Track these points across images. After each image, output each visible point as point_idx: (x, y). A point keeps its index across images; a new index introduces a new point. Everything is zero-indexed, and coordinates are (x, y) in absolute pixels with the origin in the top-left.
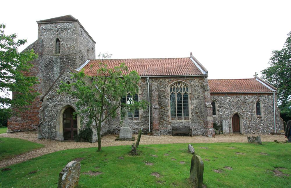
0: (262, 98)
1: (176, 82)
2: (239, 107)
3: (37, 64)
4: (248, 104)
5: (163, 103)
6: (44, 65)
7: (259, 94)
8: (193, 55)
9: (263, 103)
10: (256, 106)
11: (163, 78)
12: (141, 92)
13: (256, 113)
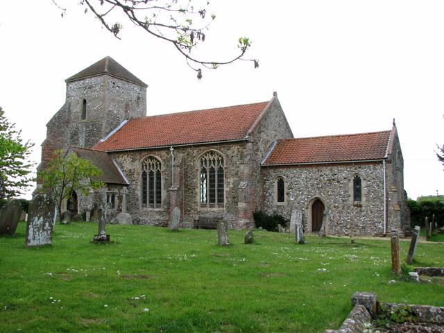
0: (363, 172)
1: (208, 152)
2: (322, 188)
3: (62, 136)
4: (338, 182)
5: (191, 184)
6: (69, 135)
7: (356, 164)
8: (279, 97)
9: (364, 180)
10: (354, 186)
11: (191, 146)
12: (165, 169)
13: (352, 199)
